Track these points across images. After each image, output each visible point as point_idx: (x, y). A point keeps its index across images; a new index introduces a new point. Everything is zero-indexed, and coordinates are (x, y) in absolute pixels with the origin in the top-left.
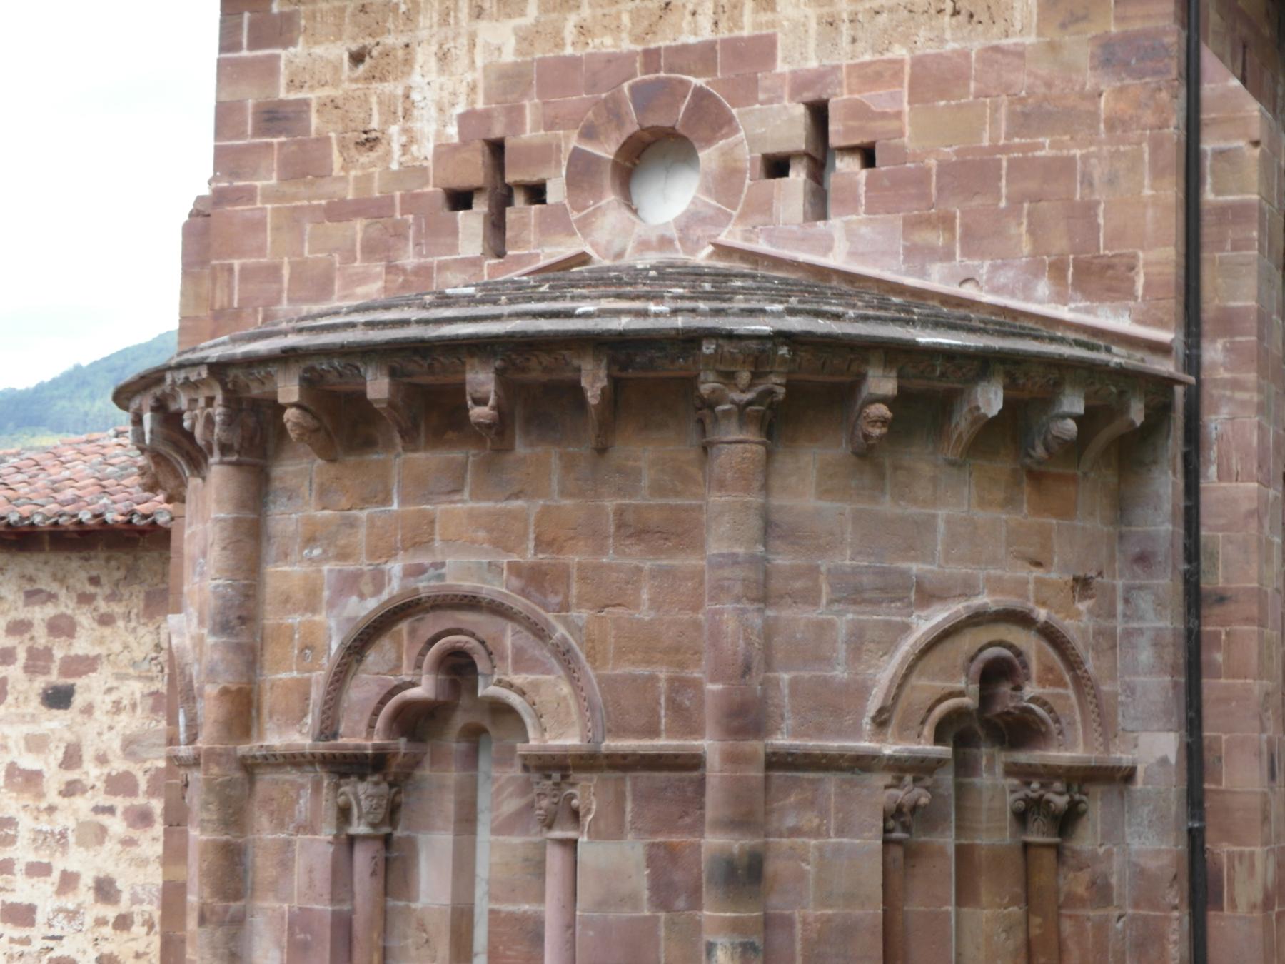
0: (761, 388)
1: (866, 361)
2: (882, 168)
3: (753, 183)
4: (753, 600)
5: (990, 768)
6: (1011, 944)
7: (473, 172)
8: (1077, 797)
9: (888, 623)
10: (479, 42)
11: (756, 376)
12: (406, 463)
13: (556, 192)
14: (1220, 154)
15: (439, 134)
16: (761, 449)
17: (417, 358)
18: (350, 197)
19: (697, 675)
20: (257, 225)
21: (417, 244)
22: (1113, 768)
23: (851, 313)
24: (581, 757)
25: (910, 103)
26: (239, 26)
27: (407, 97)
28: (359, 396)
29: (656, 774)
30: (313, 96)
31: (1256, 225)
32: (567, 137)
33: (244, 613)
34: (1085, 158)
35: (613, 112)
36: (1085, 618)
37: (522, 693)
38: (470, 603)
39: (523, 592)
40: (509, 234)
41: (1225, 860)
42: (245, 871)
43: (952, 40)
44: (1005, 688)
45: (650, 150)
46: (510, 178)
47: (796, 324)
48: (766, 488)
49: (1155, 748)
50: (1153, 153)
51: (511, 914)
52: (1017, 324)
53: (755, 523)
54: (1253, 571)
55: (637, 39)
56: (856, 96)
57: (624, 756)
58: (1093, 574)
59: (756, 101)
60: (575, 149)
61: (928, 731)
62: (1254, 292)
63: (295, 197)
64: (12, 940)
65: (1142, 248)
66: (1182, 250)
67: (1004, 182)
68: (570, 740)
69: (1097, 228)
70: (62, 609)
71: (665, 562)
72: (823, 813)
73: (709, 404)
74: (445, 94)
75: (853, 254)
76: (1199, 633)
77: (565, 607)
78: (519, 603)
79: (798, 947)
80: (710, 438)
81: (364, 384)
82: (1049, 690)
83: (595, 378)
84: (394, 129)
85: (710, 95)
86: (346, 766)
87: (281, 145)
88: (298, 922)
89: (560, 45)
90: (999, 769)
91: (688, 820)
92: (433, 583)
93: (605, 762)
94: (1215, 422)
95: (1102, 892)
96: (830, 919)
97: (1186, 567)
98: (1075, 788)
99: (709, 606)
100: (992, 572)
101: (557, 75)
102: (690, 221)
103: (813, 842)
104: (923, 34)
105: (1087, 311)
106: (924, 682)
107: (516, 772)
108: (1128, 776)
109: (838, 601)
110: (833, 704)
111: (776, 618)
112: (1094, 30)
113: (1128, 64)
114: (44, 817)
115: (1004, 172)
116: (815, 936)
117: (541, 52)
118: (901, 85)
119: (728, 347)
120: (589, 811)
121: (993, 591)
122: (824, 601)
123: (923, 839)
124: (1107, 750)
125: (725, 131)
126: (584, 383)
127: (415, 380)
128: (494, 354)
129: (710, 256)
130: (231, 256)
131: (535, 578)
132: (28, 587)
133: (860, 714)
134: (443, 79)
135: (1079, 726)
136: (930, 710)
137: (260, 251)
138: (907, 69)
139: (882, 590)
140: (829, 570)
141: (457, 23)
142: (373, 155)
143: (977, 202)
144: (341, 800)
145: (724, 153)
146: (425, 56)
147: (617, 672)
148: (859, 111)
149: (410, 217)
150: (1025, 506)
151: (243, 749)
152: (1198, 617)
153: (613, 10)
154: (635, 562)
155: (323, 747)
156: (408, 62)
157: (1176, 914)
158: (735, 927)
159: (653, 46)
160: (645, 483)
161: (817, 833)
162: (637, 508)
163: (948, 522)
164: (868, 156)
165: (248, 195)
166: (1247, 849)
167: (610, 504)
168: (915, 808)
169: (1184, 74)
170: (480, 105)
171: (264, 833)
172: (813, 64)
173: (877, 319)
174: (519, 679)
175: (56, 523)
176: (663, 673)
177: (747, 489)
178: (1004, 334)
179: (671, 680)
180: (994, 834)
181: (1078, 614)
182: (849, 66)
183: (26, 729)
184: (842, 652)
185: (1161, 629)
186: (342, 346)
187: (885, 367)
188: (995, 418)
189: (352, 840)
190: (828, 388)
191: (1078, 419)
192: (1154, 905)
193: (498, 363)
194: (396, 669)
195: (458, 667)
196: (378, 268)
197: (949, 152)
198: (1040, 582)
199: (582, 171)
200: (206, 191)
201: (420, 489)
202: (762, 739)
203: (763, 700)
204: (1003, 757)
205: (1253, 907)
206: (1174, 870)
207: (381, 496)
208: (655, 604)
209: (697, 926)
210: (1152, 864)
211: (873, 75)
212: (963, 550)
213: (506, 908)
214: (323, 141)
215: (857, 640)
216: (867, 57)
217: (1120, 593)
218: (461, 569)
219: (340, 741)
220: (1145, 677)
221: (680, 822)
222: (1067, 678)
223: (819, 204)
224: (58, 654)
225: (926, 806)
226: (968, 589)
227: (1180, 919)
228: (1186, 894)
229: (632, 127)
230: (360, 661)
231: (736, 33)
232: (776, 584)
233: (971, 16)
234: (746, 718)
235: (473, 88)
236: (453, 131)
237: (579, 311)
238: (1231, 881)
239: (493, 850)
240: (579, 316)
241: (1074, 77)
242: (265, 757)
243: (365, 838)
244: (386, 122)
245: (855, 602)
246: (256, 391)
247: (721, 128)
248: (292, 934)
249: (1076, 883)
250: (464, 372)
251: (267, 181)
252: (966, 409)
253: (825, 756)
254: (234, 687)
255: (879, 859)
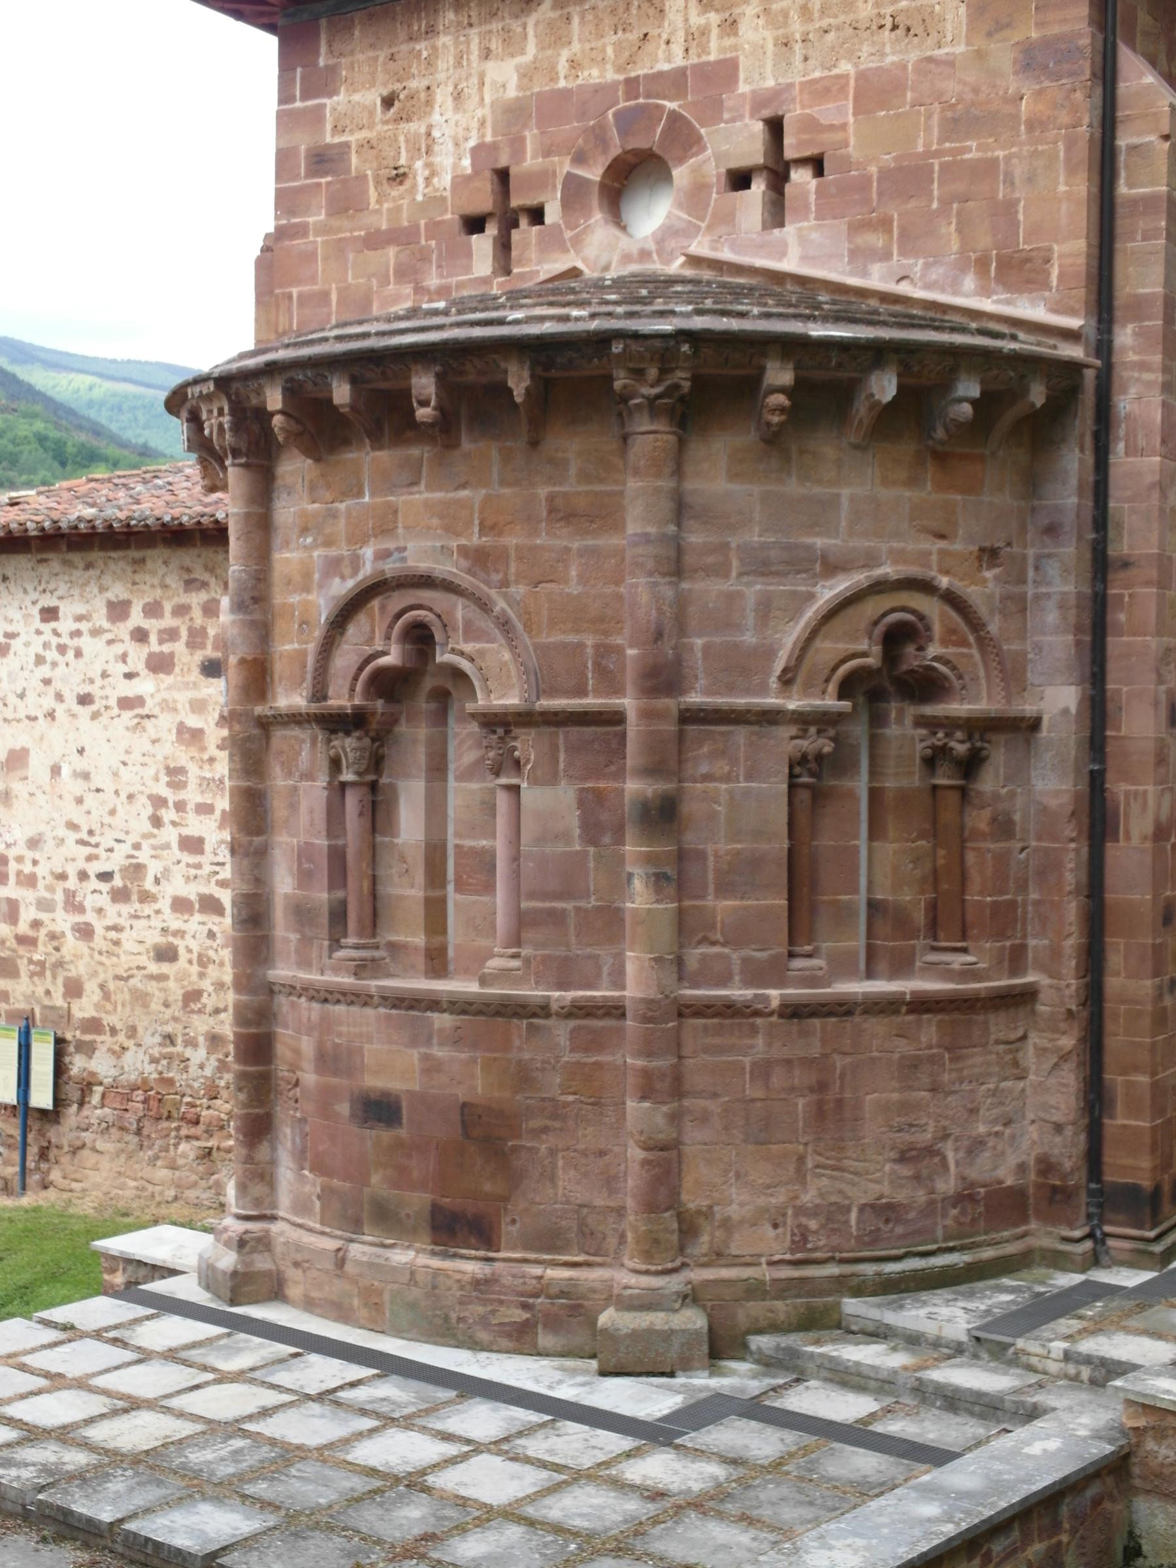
0: (668, 383)
1: (764, 355)
2: (829, 177)
3: (716, 197)
4: (664, 575)
5: (900, 720)
6: (918, 873)
7: (483, 200)
8: (979, 744)
9: (794, 593)
10: (487, 80)
11: (664, 372)
12: (368, 460)
13: (552, 214)
14: (1133, 148)
15: (455, 166)
16: (672, 438)
17: (371, 366)
18: (384, 227)
19: (619, 641)
20: (310, 257)
21: (439, 267)
22: (1015, 719)
23: (756, 311)
24: (519, 714)
25: (854, 114)
26: (293, 80)
27: (429, 134)
28: (327, 402)
29: (585, 729)
30: (352, 138)
31: (1165, 215)
32: (561, 163)
33: (256, 594)
34: (1008, 159)
35: (599, 137)
36: (991, 585)
37: (472, 660)
38: (426, 581)
39: (469, 571)
40: (514, 253)
41: (1122, 798)
42: (266, 812)
43: (893, 53)
44: (910, 649)
45: (630, 174)
46: (515, 203)
47: (699, 323)
48: (678, 472)
49: (1058, 700)
50: (1068, 149)
51: (472, 848)
52: (947, 318)
53: (667, 505)
54: (1154, 538)
55: (619, 69)
56: (808, 111)
57: (556, 714)
58: (1001, 544)
59: (721, 120)
60: (568, 173)
61: (832, 688)
62: (1162, 279)
63: (340, 230)
64: (188, 865)
65: (1056, 241)
66: (1095, 242)
67: (936, 185)
68: (512, 700)
69: (1015, 224)
70: (213, 595)
71: (591, 542)
72: (734, 761)
73: (624, 399)
74: (460, 130)
75: (804, 258)
76: (1104, 596)
77: (505, 583)
78: (466, 580)
79: (711, 876)
80: (628, 429)
81: (331, 392)
82: (952, 650)
83: (520, 379)
84: (419, 164)
85: (682, 117)
86: (335, 723)
87: (328, 183)
88: (304, 853)
89: (554, 79)
90: (908, 721)
91: (613, 768)
92: (398, 565)
93: (540, 719)
94: (1125, 403)
95: (1004, 827)
96: (738, 853)
97: (1094, 536)
98: (977, 736)
99: (630, 581)
100: (895, 545)
101: (551, 107)
102: (667, 233)
103: (724, 786)
104: (866, 49)
105: (1008, 302)
106: (827, 645)
107: (474, 727)
108: (1035, 724)
109: (747, 574)
110: (742, 666)
111: (690, 590)
112: (1017, 36)
113: (1047, 67)
114: (206, 767)
115: (936, 175)
116: (725, 867)
117: (539, 86)
118: (846, 99)
119: (635, 347)
120: (528, 760)
121: (895, 562)
122: (734, 574)
123: (833, 783)
124: (1009, 702)
125: (694, 149)
126: (511, 383)
127: (374, 386)
128: (434, 361)
129: (682, 266)
130: (290, 285)
131: (480, 559)
132: (186, 577)
133: (768, 675)
134: (458, 116)
135: (983, 681)
136: (834, 669)
137: (313, 279)
138: (852, 83)
139: (788, 563)
140: (738, 547)
141: (469, 65)
142: (402, 188)
143: (912, 204)
144: (332, 752)
145: (695, 170)
146: (443, 96)
147: (551, 640)
148: (810, 125)
149: (433, 243)
150: (929, 484)
151: (259, 710)
152: (1104, 581)
153: (599, 44)
154: (565, 543)
155: (314, 708)
156: (429, 103)
157: (1073, 845)
158: (649, 859)
159: (633, 74)
160: (573, 471)
161: (727, 778)
162: (566, 494)
163: (852, 499)
164: (817, 165)
165: (301, 231)
166: (1141, 788)
167: (543, 491)
168: (820, 757)
169: (1100, 74)
170: (489, 138)
171: (279, 781)
172: (770, 83)
173: (780, 316)
174: (468, 648)
175: (199, 523)
176: (590, 641)
177: (658, 475)
178: (483, 310)
179: (597, 647)
180: (902, 778)
181: (984, 581)
182: (801, 83)
183: (190, 694)
184: (750, 619)
185: (1065, 593)
186: (310, 358)
187: (782, 360)
188: (889, 404)
189: (343, 786)
190: (722, 379)
191: (974, 403)
192: (1054, 839)
193: (438, 368)
194: (370, 640)
195: (420, 638)
196: (408, 289)
197: (887, 159)
198: (942, 553)
199: (574, 191)
200: (271, 229)
201: (386, 484)
202: (675, 697)
203: (678, 661)
204: (912, 711)
205: (1145, 838)
206: (1072, 808)
207: (355, 490)
208: (583, 579)
209: (621, 859)
210: (1053, 803)
211: (821, 91)
212: (862, 526)
213: (469, 843)
214: (362, 178)
215: (765, 609)
216: (817, 74)
217: (1031, 561)
218: (419, 553)
219: (330, 702)
220: (1052, 637)
221: (607, 770)
222: (971, 639)
223: (776, 212)
224: (211, 632)
225: (829, 754)
226: (871, 560)
227: (1077, 851)
228: (1085, 828)
229: (615, 151)
230: (342, 634)
231: (704, 58)
232: (689, 560)
233: (908, 29)
234: (663, 678)
235: (483, 123)
236: (467, 162)
237: (510, 318)
238: (1127, 815)
239: (461, 794)
240: (510, 323)
241: (998, 82)
242: (274, 716)
243: (353, 784)
244: (412, 159)
245: (763, 574)
246: (254, 401)
247: (691, 147)
248: (300, 864)
249: (978, 819)
250: (409, 378)
251: (317, 217)
252: (863, 397)
253: (733, 711)
254: (249, 658)
255: (785, 800)
